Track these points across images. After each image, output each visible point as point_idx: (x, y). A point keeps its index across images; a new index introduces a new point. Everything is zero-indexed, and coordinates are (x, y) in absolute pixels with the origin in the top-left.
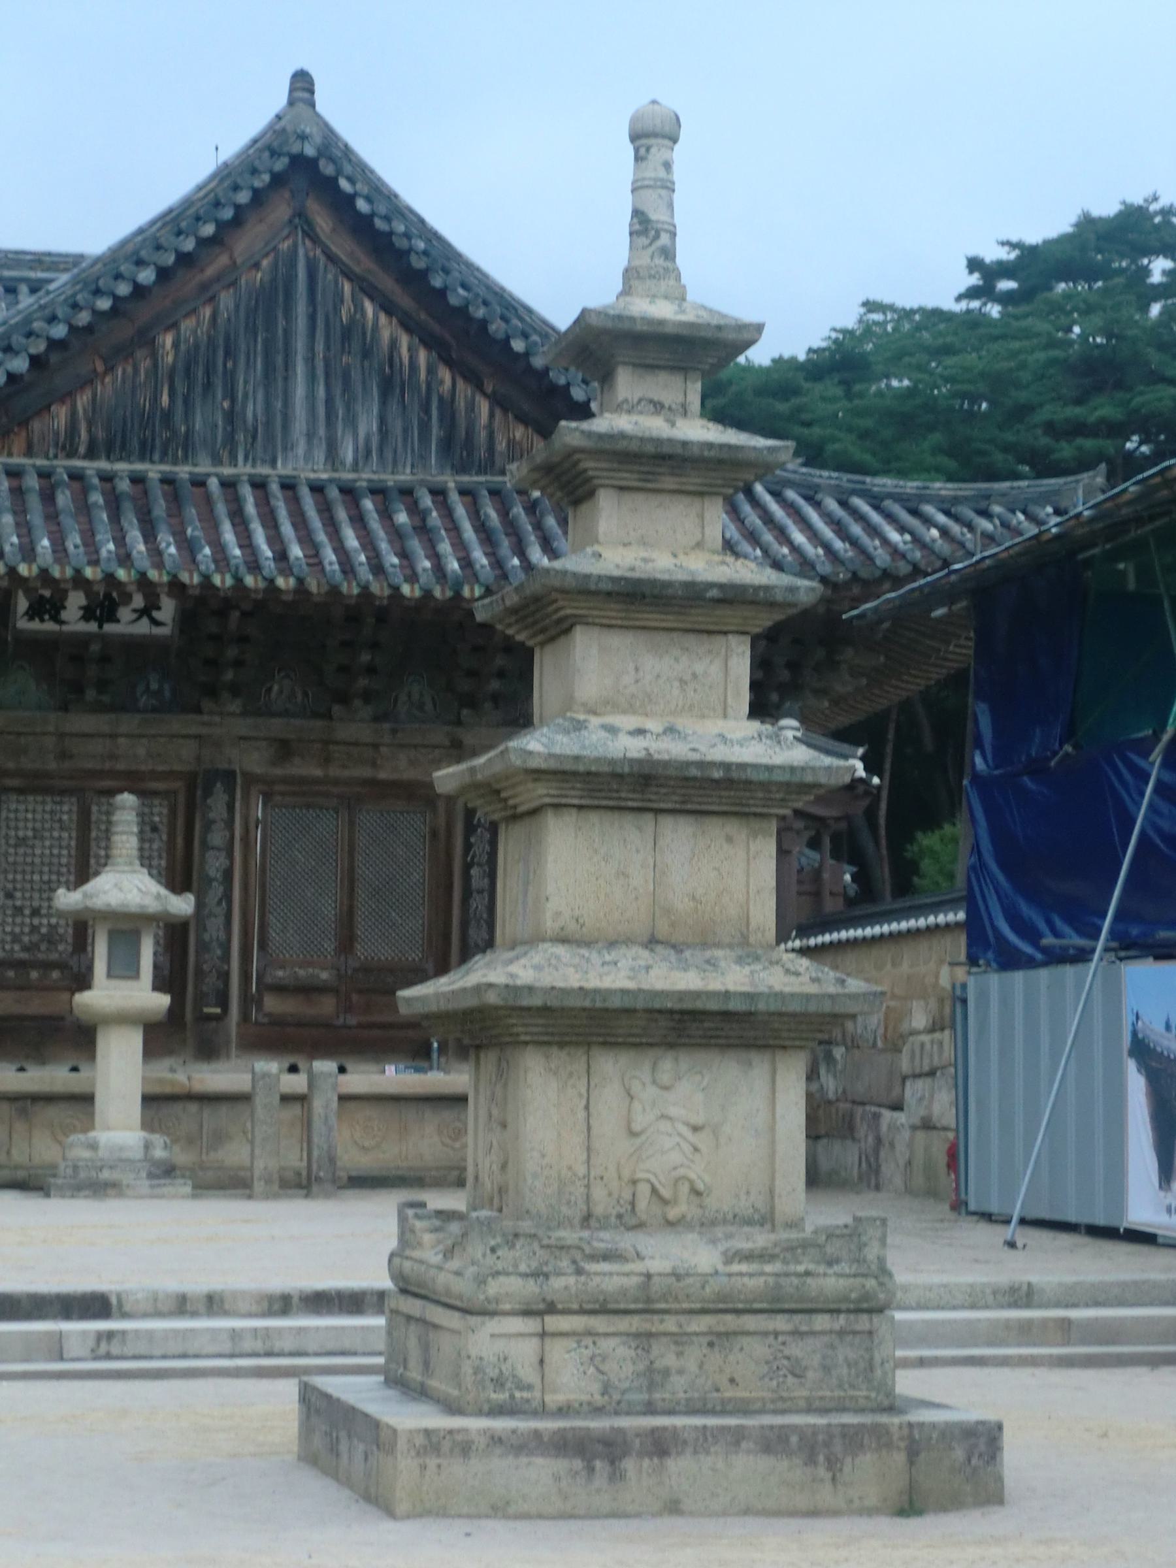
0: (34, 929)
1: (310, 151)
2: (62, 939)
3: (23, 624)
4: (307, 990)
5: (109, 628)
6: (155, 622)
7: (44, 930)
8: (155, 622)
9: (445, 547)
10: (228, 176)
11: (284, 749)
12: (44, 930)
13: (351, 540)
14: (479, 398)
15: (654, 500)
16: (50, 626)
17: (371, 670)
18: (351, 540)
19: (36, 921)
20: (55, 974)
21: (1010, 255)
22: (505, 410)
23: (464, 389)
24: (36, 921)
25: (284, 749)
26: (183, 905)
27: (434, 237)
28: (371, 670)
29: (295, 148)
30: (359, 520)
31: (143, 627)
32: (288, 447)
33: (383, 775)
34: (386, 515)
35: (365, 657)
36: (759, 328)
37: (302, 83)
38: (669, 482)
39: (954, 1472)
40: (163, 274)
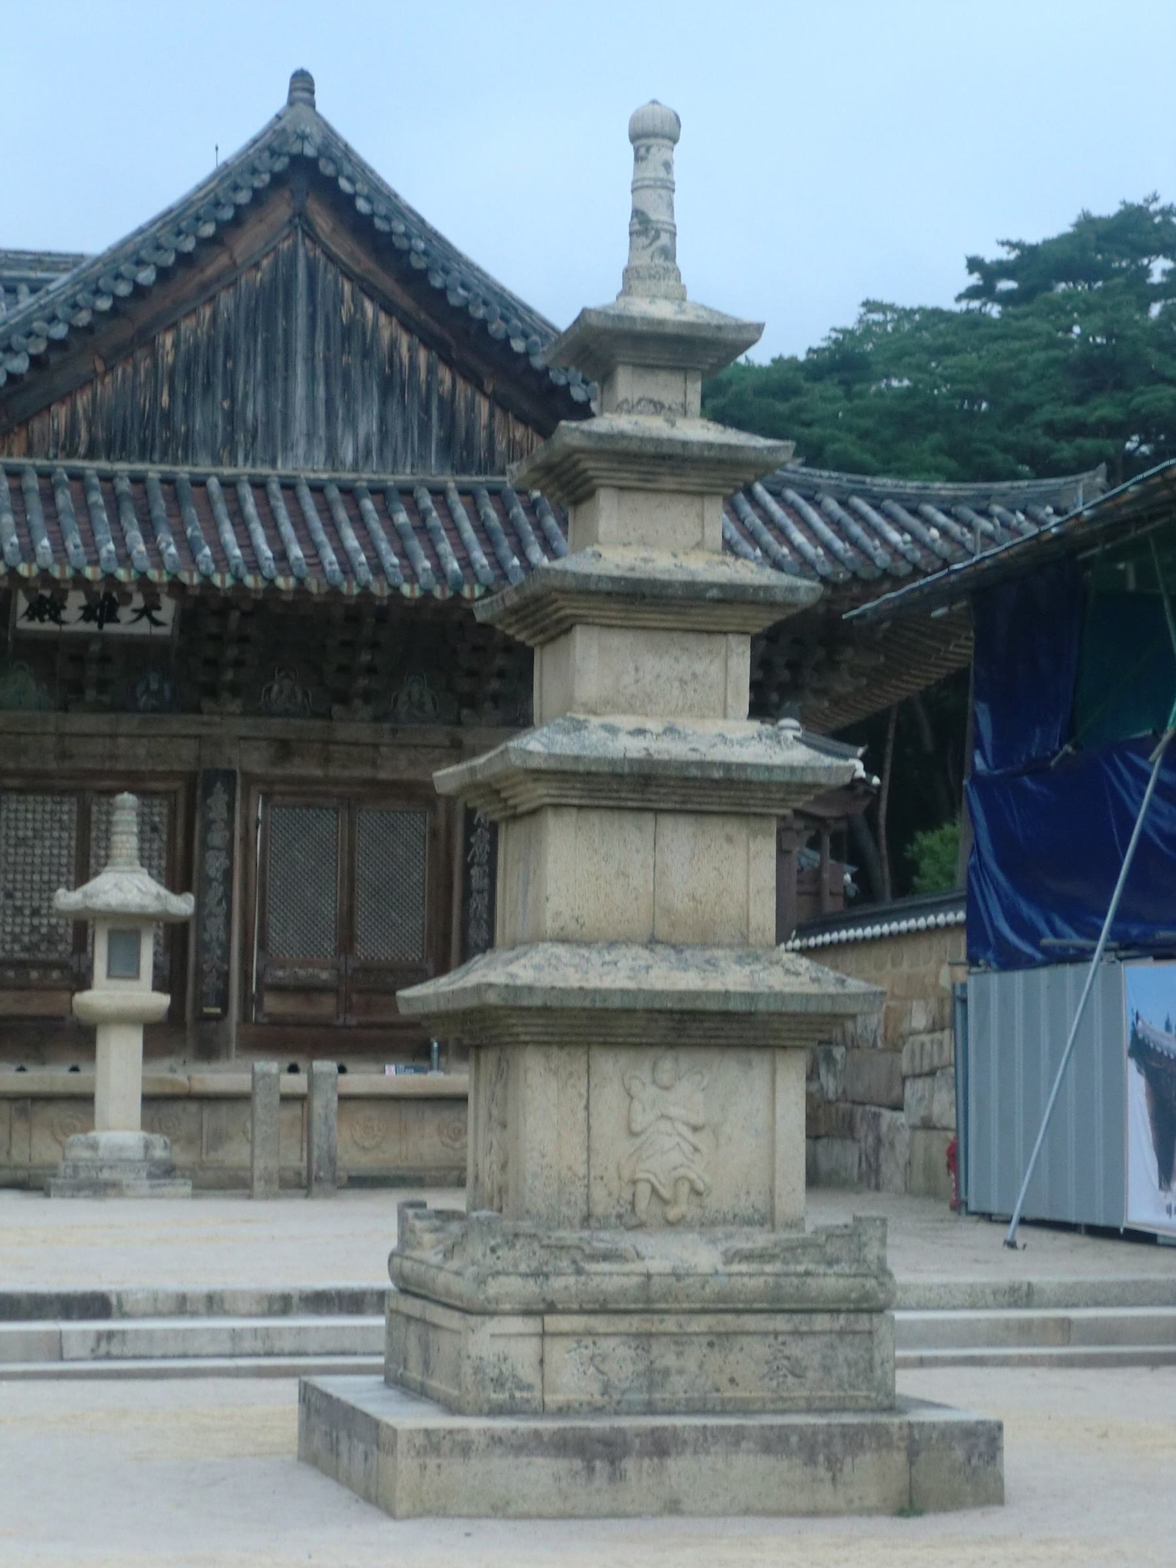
0: (34, 929)
1: (310, 151)
2: (62, 939)
3: (23, 624)
4: (307, 990)
5: (109, 628)
6: (155, 622)
7: (44, 930)
8: (155, 622)
9: (445, 547)
10: (228, 176)
11: (284, 749)
12: (44, 930)
13: (351, 540)
14: (479, 398)
15: (654, 500)
16: (50, 626)
17: (371, 670)
18: (351, 540)
19: (36, 921)
20: (55, 974)
21: (1010, 255)
22: (505, 410)
23: (464, 389)
24: (36, 921)
25: (284, 749)
26: (183, 905)
27: (434, 237)
28: (371, 670)
29: (295, 148)
30: (359, 520)
31: (143, 627)
32: (288, 447)
33: (383, 775)
34: (386, 515)
35: (365, 657)
36: (759, 328)
37: (302, 83)
38: (669, 482)
39: (954, 1472)
40: (163, 274)
